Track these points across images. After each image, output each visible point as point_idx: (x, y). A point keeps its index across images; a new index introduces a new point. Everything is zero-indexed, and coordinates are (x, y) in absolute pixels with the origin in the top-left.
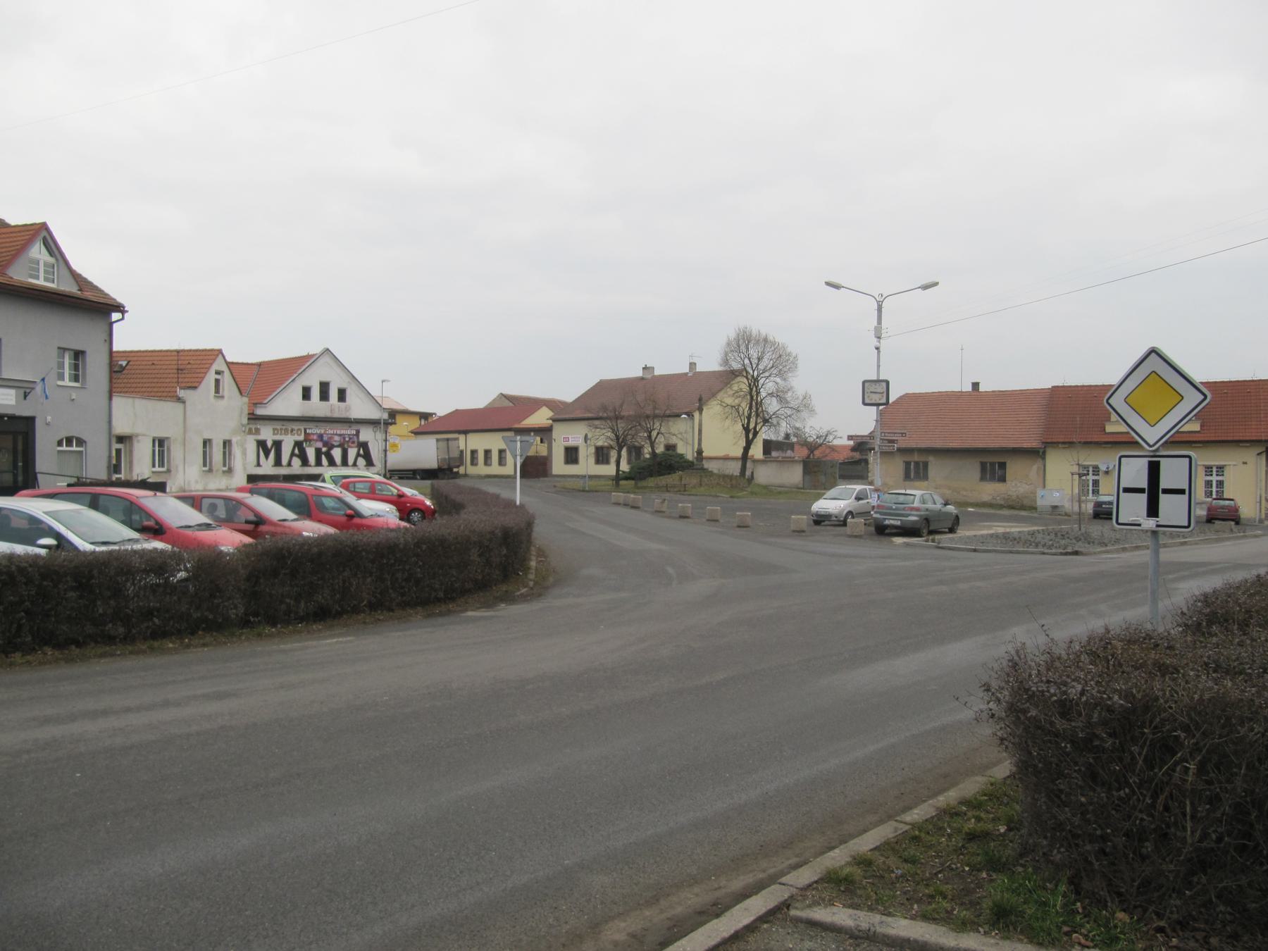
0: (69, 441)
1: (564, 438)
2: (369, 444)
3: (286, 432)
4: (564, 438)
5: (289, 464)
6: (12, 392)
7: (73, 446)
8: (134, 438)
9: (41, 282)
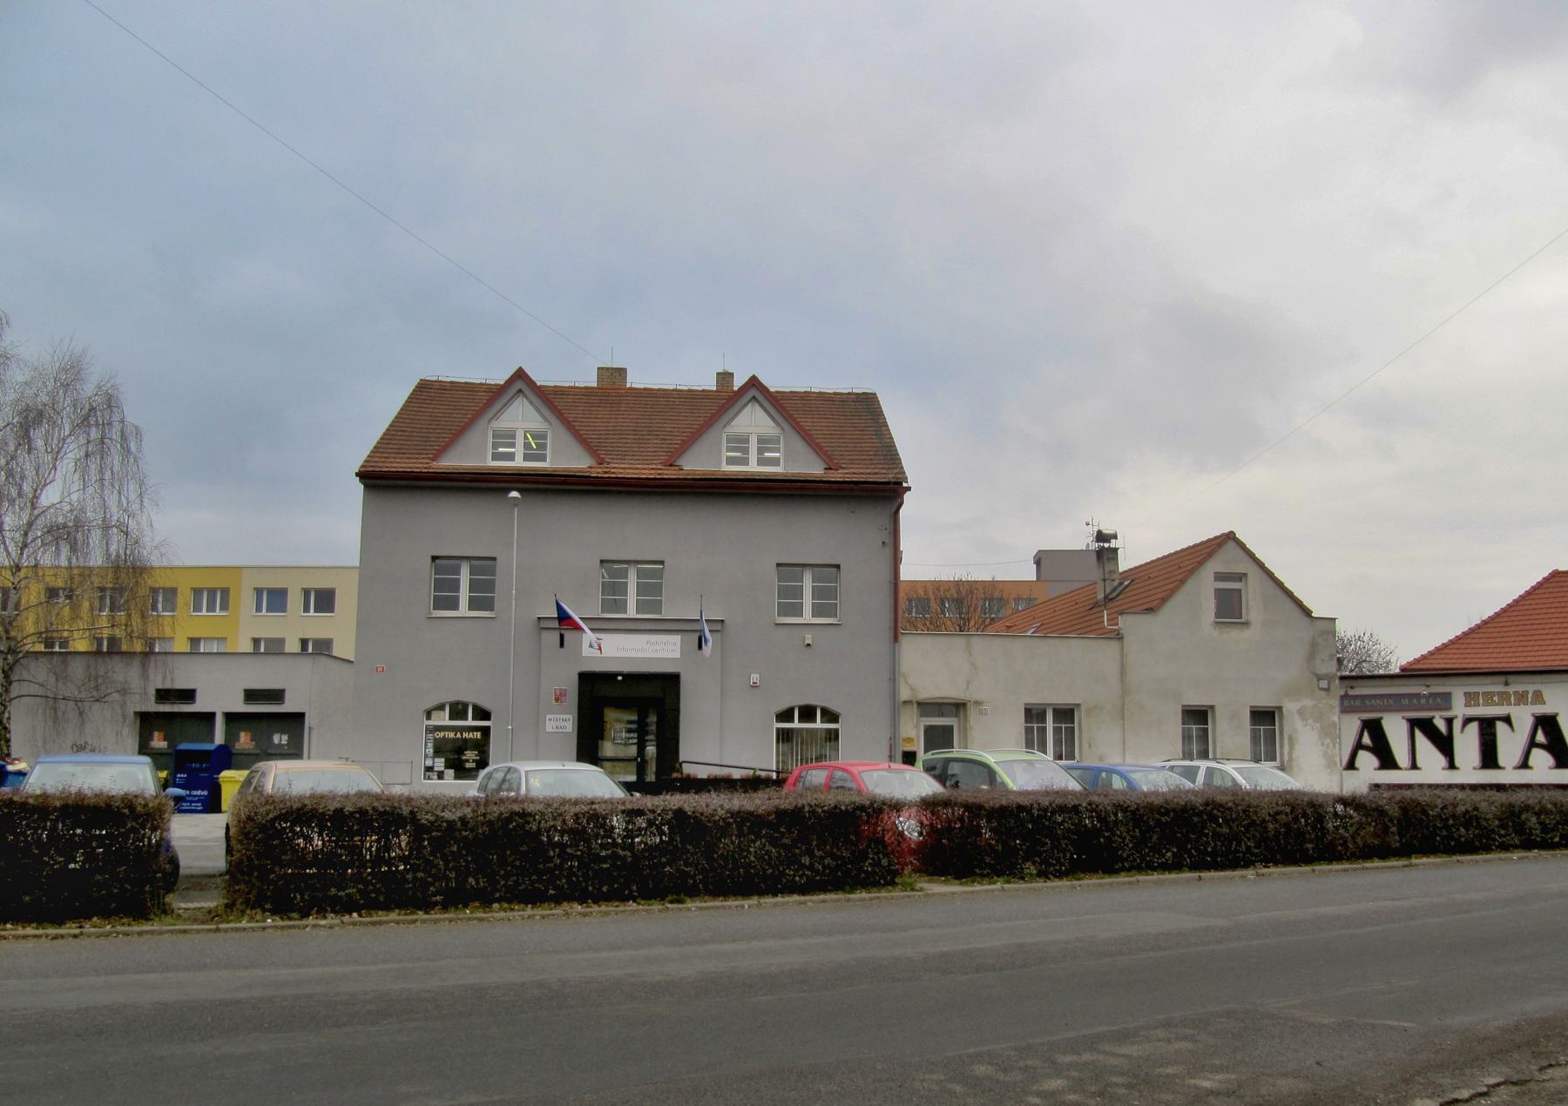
0: (808, 713)
1: (425, 778)
2: (1560, 719)
3: (1521, 698)
4: (425, 778)
5: (1524, 765)
6: (676, 639)
7: (467, 719)
8: (968, 704)
9: (753, 468)
